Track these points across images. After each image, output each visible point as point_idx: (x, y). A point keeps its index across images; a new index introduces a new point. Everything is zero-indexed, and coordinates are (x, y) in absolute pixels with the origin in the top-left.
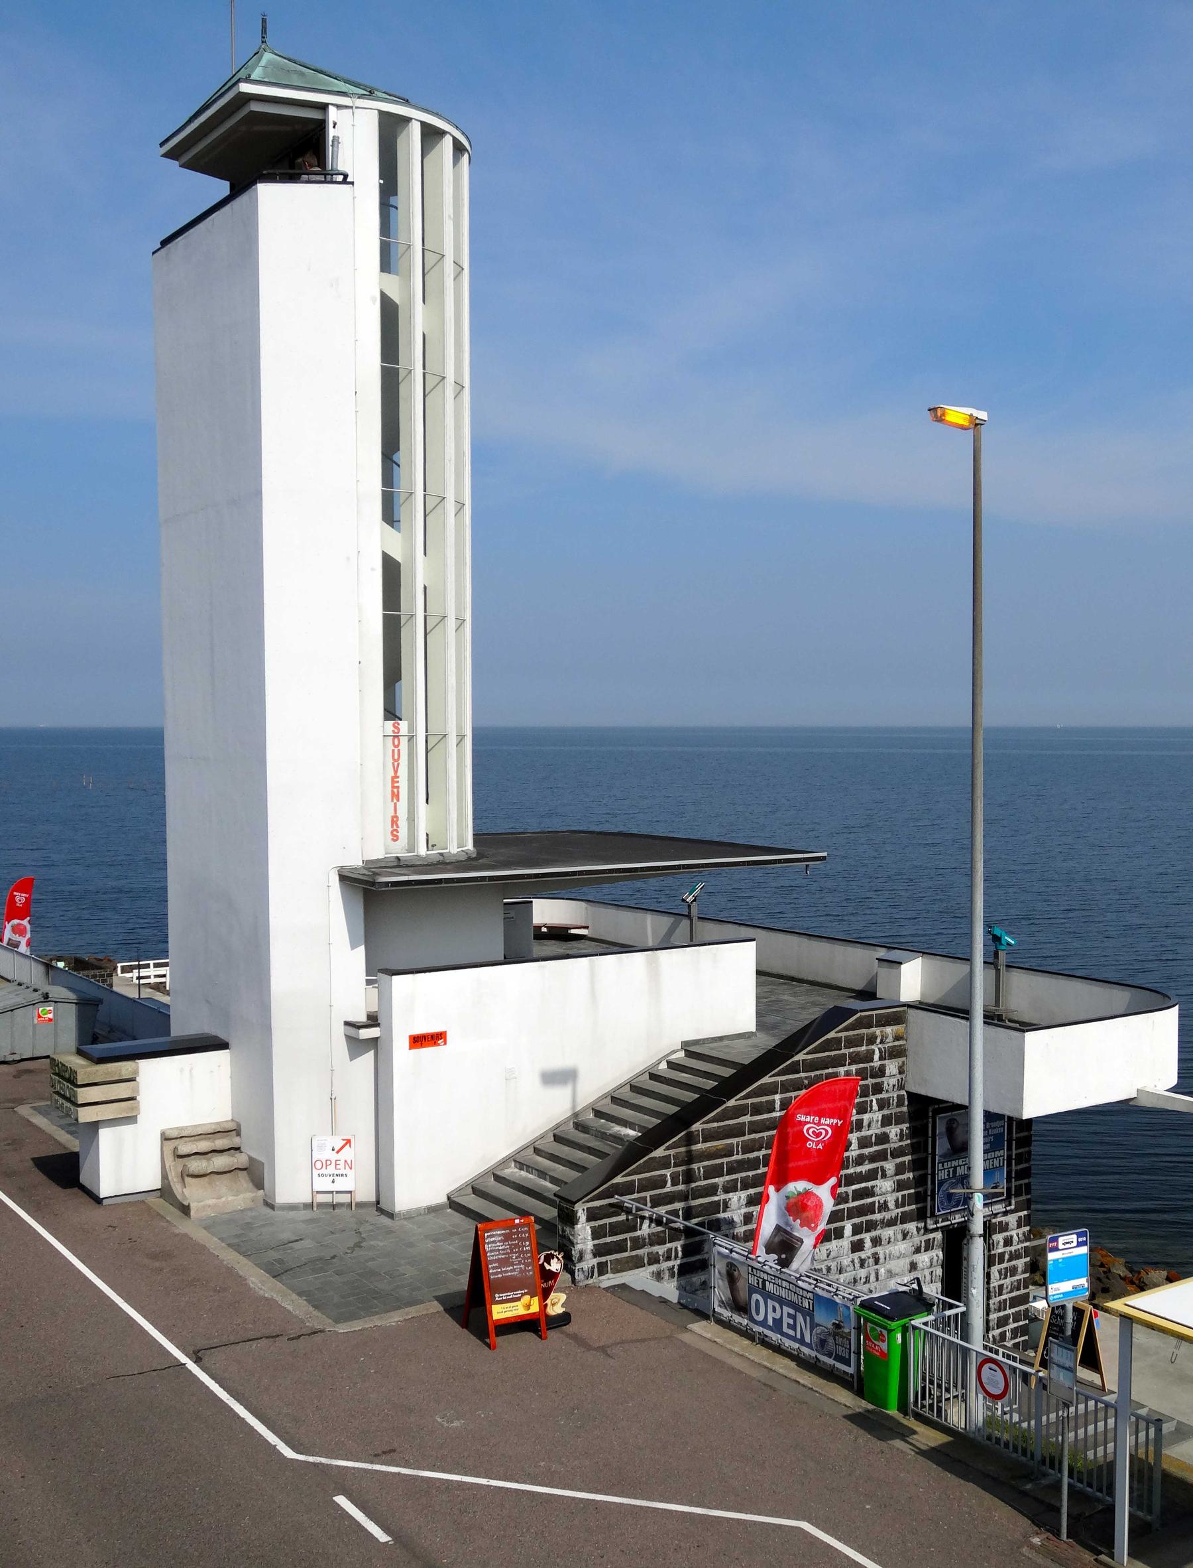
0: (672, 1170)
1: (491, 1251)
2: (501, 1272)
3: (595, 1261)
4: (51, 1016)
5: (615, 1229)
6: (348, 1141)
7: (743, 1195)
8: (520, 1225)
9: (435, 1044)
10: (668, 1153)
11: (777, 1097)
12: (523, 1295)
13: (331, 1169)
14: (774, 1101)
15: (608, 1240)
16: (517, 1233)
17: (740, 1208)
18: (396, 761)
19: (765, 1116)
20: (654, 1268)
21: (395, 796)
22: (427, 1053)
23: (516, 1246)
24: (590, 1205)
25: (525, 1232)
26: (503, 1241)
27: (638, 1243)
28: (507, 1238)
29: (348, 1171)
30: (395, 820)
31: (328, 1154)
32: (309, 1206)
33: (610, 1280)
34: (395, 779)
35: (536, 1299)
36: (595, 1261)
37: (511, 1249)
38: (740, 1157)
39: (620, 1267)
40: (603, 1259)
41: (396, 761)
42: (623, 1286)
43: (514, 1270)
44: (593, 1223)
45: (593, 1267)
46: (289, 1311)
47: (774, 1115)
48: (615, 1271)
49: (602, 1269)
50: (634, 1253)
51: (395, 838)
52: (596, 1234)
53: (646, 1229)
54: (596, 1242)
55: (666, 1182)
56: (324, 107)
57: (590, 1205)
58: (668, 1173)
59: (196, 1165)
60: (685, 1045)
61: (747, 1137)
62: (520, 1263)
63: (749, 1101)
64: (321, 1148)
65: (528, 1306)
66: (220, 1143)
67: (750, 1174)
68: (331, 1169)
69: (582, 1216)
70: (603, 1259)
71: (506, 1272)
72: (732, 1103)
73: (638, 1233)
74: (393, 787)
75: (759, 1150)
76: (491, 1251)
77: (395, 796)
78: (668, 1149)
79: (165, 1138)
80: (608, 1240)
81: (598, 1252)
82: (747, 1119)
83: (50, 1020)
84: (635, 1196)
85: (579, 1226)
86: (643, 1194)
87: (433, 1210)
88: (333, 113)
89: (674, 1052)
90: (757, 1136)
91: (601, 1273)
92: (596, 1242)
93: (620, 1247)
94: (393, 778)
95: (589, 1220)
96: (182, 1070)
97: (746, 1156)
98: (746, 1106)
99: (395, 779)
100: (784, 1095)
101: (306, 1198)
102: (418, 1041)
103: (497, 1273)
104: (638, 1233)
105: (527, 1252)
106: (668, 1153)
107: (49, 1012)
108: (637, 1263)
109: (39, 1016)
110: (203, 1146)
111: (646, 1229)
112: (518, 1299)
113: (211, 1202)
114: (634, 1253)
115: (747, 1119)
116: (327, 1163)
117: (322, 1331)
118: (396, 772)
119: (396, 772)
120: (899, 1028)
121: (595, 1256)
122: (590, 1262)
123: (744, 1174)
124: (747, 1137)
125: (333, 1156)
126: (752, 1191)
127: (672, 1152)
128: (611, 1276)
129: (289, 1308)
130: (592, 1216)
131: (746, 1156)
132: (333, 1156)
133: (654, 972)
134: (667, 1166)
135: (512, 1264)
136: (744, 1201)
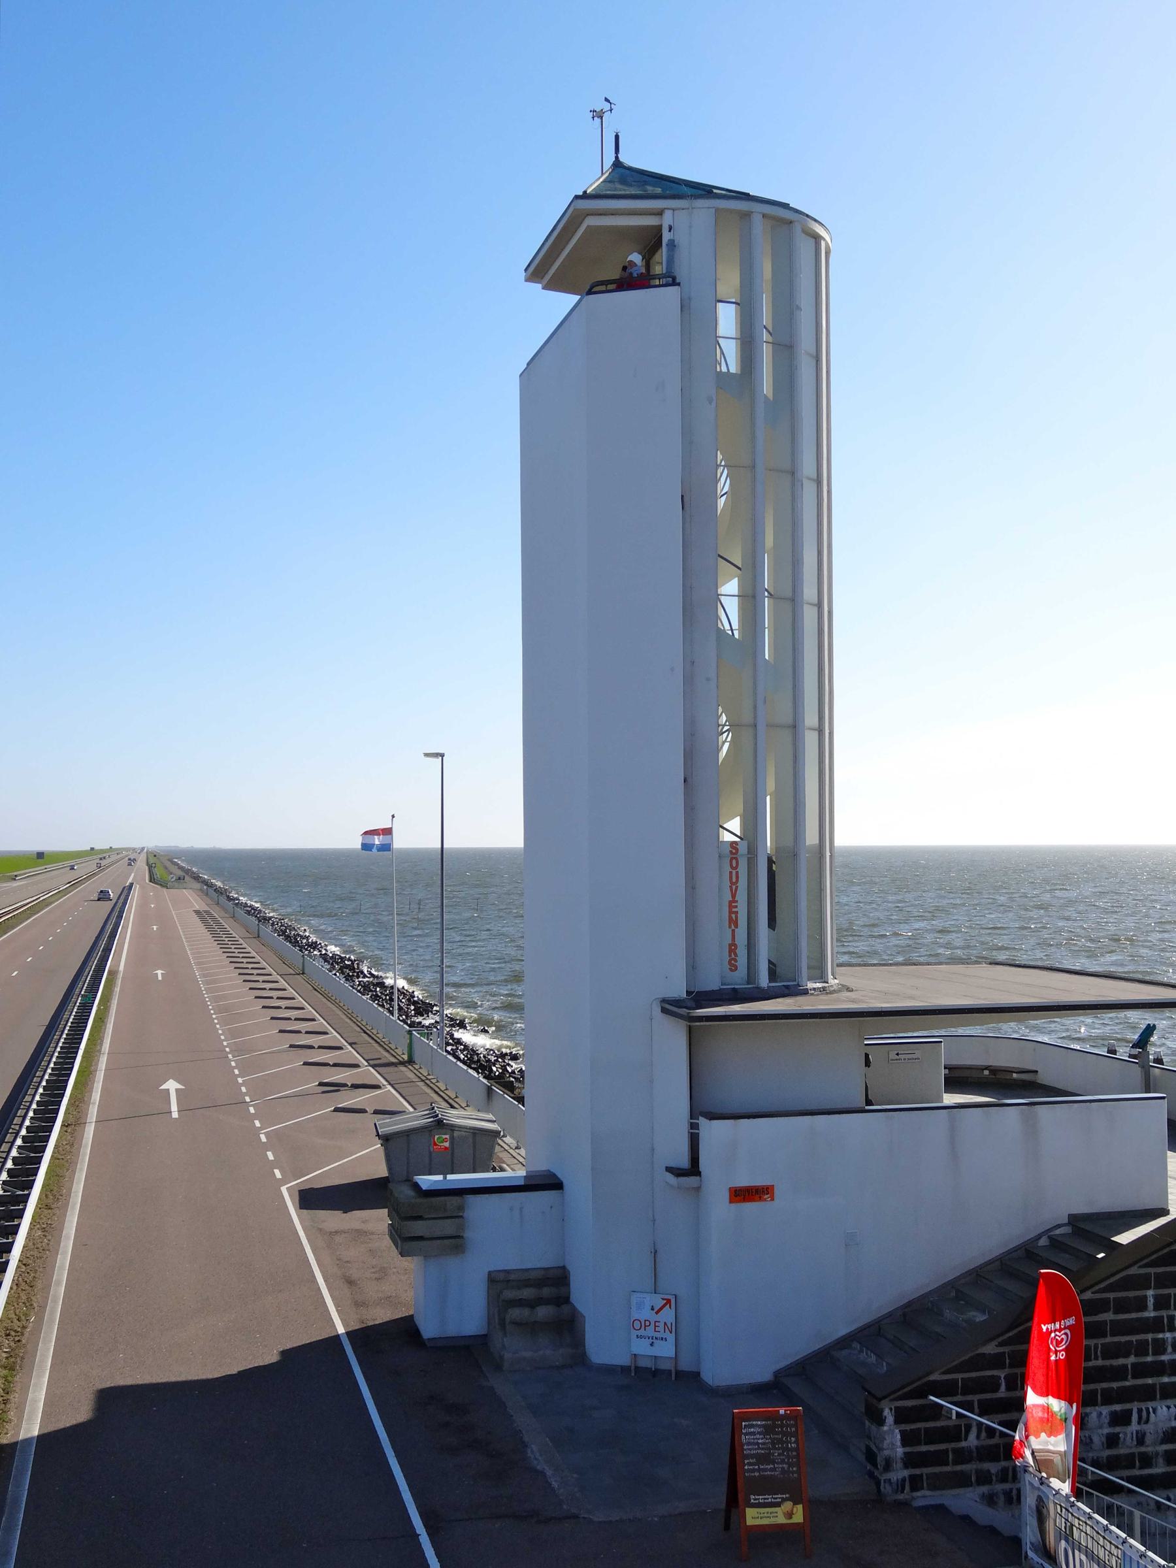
0: (1007, 1371)
1: (749, 1444)
2: (759, 1470)
3: (906, 1473)
4: (447, 1144)
5: (933, 1436)
6: (669, 1301)
7: (1105, 1410)
8: (785, 1417)
9: (760, 1199)
10: (1001, 1350)
11: (1150, 1293)
12: (784, 1500)
13: (650, 1331)
14: (1146, 1297)
15: (924, 1448)
16: (782, 1426)
17: (1101, 1427)
18: (734, 884)
19: (1134, 1315)
20: (984, 1489)
21: (734, 922)
22: (750, 1208)
23: (780, 1441)
24: (900, 1403)
25: (792, 1426)
26: (764, 1434)
27: (962, 1456)
28: (768, 1430)
29: (667, 1335)
30: (733, 948)
31: (646, 1314)
32: (625, 1370)
33: (924, 1497)
34: (732, 903)
35: (800, 1507)
36: (906, 1473)
37: (773, 1443)
38: (1100, 1362)
39: (937, 1483)
40: (917, 1471)
41: (734, 884)
42: (941, 1509)
43: (774, 1469)
44: (904, 1427)
45: (904, 1480)
46: (553, 1489)
47: (1146, 1314)
48: (933, 1487)
49: (915, 1483)
50: (958, 1468)
51: (734, 968)
52: (907, 1439)
53: (972, 1441)
54: (908, 1449)
55: (999, 1385)
57: (900, 1403)
58: (1002, 1374)
59: (515, 1313)
60: (1074, 1220)
61: (1109, 1339)
62: (783, 1462)
63: (1112, 1295)
64: (640, 1306)
65: (789, 1515)
66: (546, 1292)
67: (1115, 1385)
68: (650, 1331)
70: (917, 1471)
71: (765, 1470)
73: (963, 1444)
74: (731, 912)
75: (1127, 1356)
76: (749, 1444)
78: (1000, 1345)
80: (924, 1448)
81: (910, 1461)
82: (1109, 1316)
83: (446, 1148)
84: (959, 1398)
85: (885, 1428)
86: (969, 1398)
89: (1059, 1226)
90: (1124, 1339)
91: (914, 1488)
92: (908, 1449)
93: (939, 1459)
94: (731, 902)
95: (896, 1422)
96: (511, 1209)
97: (1108, 1363)
98: (1107, 1301)
99: (732, 903)
100: (1160, 1292)
101: (623, 1360)
102: (742, 1195)
103: (754, 1471)
104: (963, 1444)
105: (792, 1450)
106: (1001, 1350)
107: (445, 1140)
108: (962, 1481)
109: (435, 1144)
110: (527, 1293)
111: (972, 1441)
112: (778, 1505)
113: (528, 1354)
114: (958, 1468)
115: (1109, 1316)
116: (646, 1324)
117: (576, 1517)
118: (734, 896)
119: (734, 896)
121: (906, 1466)
122: (900, 1473)
123: (1105, 1385)
124: (1109, 1339)
125: (652, 1317)
126: (1117, 1407)
127: (1006, 1349)
128: (928, 1493)
129: (555, 1485)
130: (902, 1417)
131: (1108, 1363)
132: (652, 1317)
133: (1031, 1130)
134: (1001, 1366)
135: (774, 1462)
136: (1106, 1420)
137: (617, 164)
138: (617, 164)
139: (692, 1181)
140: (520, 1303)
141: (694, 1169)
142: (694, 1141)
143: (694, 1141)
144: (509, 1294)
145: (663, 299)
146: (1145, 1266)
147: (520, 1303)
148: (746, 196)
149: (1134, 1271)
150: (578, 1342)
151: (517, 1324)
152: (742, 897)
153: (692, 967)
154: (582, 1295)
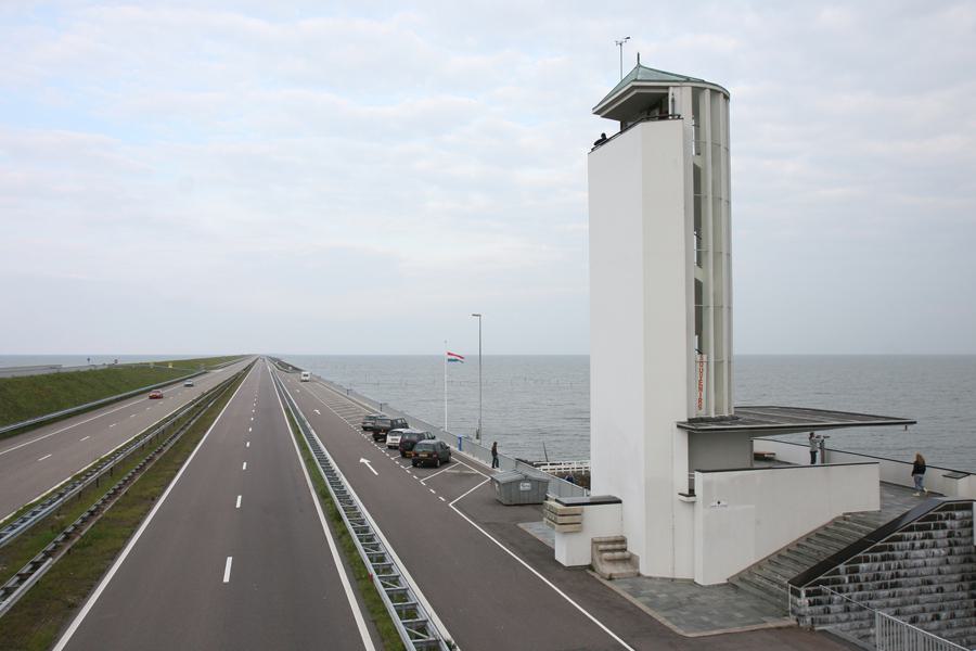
21: (701, 389)
24: (810, 588)
42: (825, 631)
51: (700, 408)
56: (667, 88)
66: (618, 546)
69: (803, 594)
72: (878, 544)
77: (701, 389)
79: (595, 543)
87: (719, 585)
88: (671, 91)
120: (966, 513)
130: (808, 594)
137: (639, 65)
138: (639, 65)
139: (692, 499)
140: (607, 551)
141: (692, 493)
142: (691, 482)
143: (691, 482)
144: (602, 547)
145: (687, 493)
146: (939, 510)
147: (607, 551)
148: (703, 82)
149: (931, 513)
150: (636, 566)
151: (606, 560)
152: (704, 378)
153: (688, 413)
154: (632, 548)
